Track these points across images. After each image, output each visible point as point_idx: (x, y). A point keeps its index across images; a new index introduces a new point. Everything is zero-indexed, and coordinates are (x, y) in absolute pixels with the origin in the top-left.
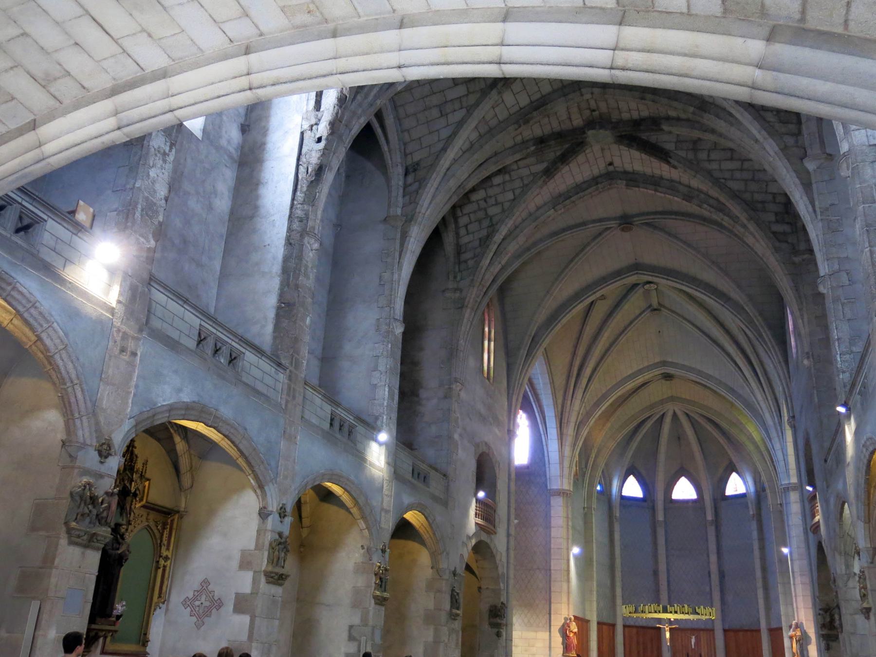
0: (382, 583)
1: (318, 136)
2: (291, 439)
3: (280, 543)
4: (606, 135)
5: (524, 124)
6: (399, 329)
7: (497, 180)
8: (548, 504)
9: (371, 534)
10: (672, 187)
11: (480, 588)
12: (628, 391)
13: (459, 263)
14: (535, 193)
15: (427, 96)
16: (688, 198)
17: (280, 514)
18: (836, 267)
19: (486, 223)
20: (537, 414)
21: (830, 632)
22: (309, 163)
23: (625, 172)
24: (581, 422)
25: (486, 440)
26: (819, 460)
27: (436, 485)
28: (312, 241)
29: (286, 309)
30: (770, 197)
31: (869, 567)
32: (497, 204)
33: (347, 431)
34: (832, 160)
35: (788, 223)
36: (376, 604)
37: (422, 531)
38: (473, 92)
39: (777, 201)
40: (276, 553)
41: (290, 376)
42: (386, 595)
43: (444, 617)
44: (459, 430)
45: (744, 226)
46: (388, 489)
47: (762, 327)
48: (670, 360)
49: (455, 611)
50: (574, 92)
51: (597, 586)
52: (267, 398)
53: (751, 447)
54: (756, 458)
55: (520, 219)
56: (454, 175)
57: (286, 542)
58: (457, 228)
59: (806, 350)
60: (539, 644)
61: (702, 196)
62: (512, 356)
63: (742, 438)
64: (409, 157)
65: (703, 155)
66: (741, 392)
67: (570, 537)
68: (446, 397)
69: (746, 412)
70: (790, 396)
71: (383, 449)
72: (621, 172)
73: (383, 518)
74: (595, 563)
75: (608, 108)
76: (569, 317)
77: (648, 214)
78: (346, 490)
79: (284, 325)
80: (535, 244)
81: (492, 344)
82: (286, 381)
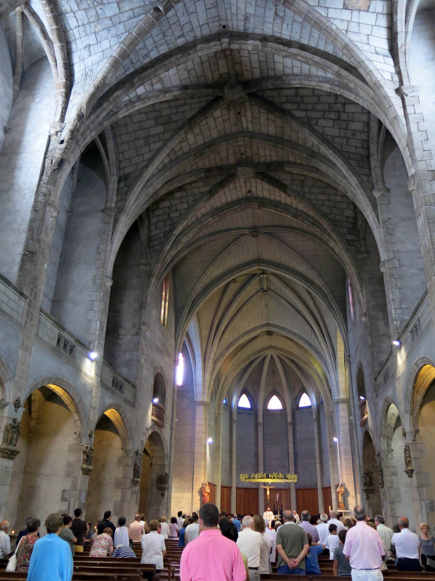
0: (88, 459)
1: (61, 139)
2: (27, 349)
3: (14, 427)
4: (249, 171)
5: (200, 156)
6: (109, 283)
7: (178, 195)
8: (195, 410)
9: (82, 423)
10: (287, 208)
11: (151, 464)
12: (245, 342)
13: (150, 247)
14: (202, 205)
15: (137, 131)
16: (295, 216)
17: (15, 405)
18: (392, 256)
19: (169, 222)
20: (190, 353)
21: (369, 488)
22: (53, 157)
23: (258, 198)
24: (216, 359)
25: (160, 365)
26: (370, 379)
27: (128, 393)
28: (53, 210)
29: (29, 255)
30: (345, 219)
31: (412, 444)
32: (176, 210)
33: (69, 348)
34: (389, 192)
35: (355, 235)
36: (83, 474)
37: (116, 424)
38: (168, 131)
40: (10, 434)
41: (29, 304)
42: (91, 467)
43: (129, 482)
44: (144, 357)
45: (329, 235)
46: (96, 392)
47: (332, 300)
48: (272, 323)
50: (232, 139)
51: (222, 463)
52: (10, 317)
53: (316, 378)
54: (318, 383)
55: (190, 222)
56: (152, 185)
57: (19, 426)
58: (150, 224)
59: (364, 311)
60: (185, 501)
61: (304, 215)
62: (179, 313)
63: (311, 372)
64: (122, 171)
65: (307, 190)
66: (312, 343)
67: (207, 432)
68: (136, 334)
69: (315, 355)
70: (348, 343)
71: (94, 364)
73: (91, 413)
75: (252, 153)
76: (215, 290)
77: (269, 226)
78: (66, 391)
79: (27, 267)
80: (198, 240)
81: (167, 303)
82: (27, 307)
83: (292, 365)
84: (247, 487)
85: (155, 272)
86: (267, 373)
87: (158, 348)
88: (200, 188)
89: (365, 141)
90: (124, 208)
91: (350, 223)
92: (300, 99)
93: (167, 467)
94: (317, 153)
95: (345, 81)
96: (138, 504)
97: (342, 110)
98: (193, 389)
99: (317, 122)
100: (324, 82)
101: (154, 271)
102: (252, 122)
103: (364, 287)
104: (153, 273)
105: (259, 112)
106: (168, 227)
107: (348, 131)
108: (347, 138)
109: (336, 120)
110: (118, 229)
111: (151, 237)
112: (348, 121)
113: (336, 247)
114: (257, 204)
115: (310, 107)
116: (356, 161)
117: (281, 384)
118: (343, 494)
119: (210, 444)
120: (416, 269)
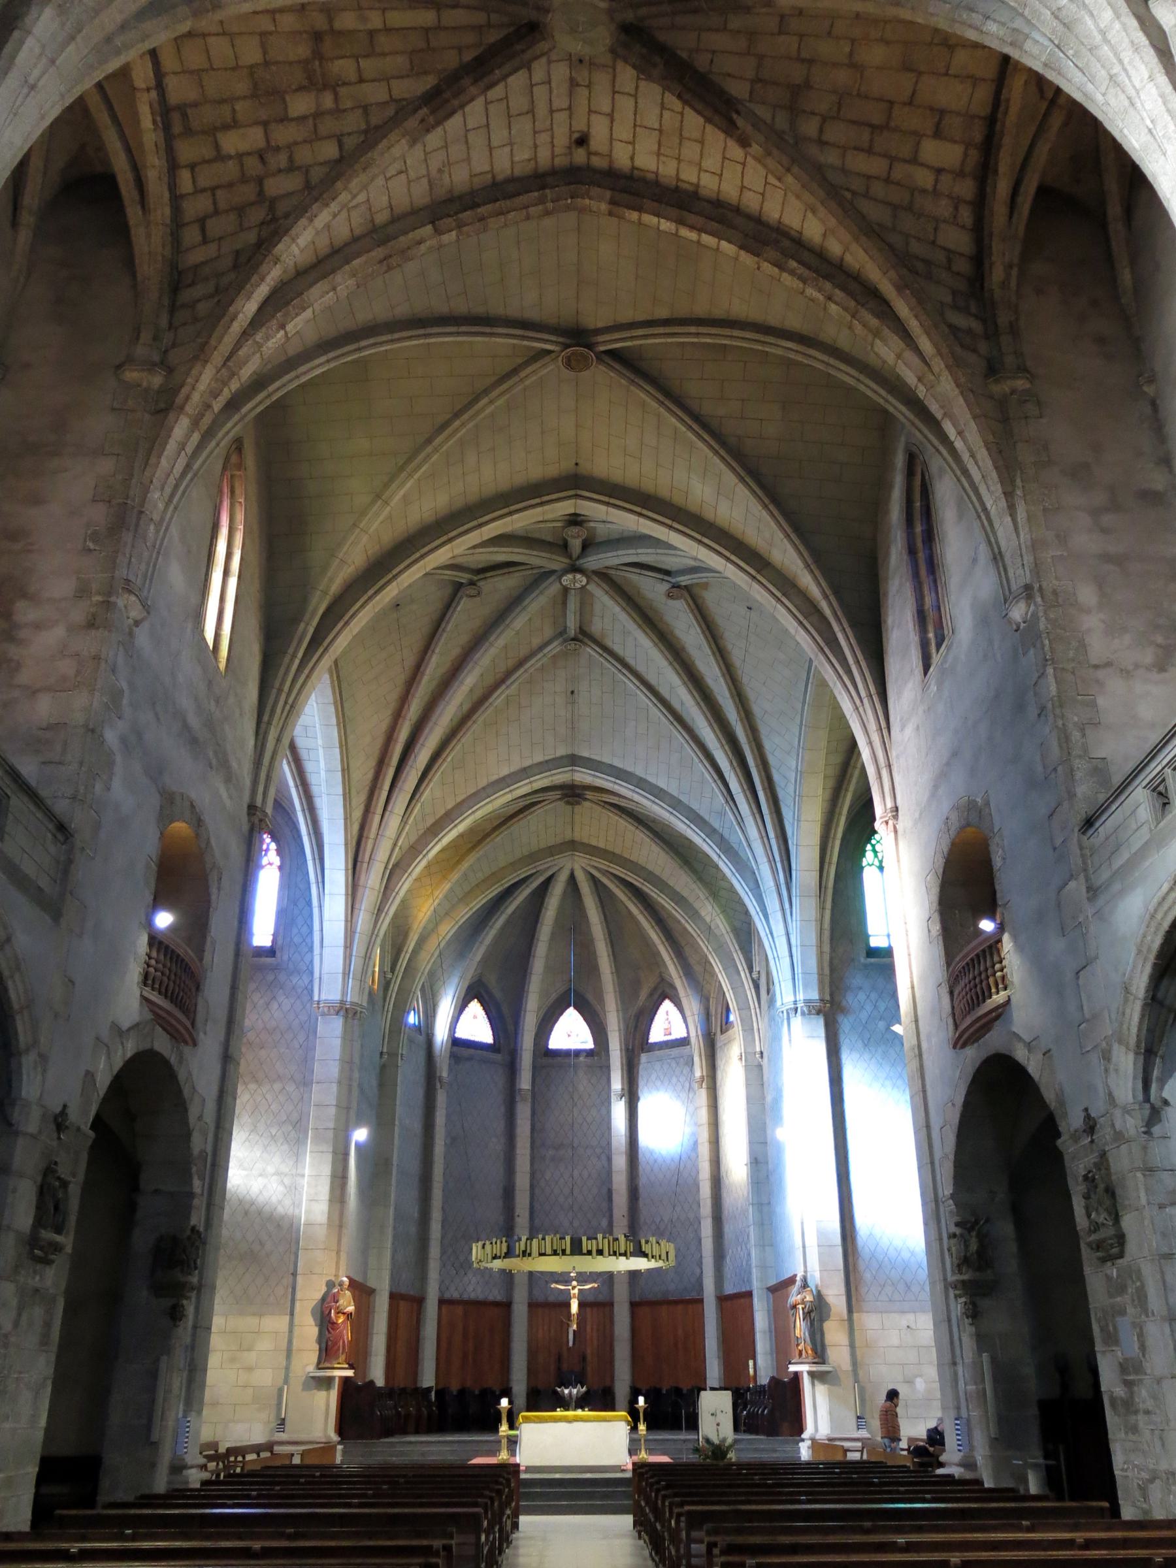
19: (257, 215)
24: (396, 865)
25: (193, 795)
30: (940, 257)
32: (292, 168)
39: (955, 268)
48: (585, 754)
49: (47, 1235)
60: (265, 1344)
61: (786, 243)
65: (810, 127)
66: (716, 825)
67: (354, 1105)
81: (233, 582)
83: (634, 909)
84: (473, 1296)
85: (188, 398)
87: (186, 726)
88: (394, 83)
91: (958, 274)
93: (199, 1203)
96: (54, 1348)
98: (312, 962)
101: (184, 391)
103: (1019, 492)
106: (255, 231)
111: (180, 273)
114: (608, 194)
118: (809, 1312)
119: (357, 1144)
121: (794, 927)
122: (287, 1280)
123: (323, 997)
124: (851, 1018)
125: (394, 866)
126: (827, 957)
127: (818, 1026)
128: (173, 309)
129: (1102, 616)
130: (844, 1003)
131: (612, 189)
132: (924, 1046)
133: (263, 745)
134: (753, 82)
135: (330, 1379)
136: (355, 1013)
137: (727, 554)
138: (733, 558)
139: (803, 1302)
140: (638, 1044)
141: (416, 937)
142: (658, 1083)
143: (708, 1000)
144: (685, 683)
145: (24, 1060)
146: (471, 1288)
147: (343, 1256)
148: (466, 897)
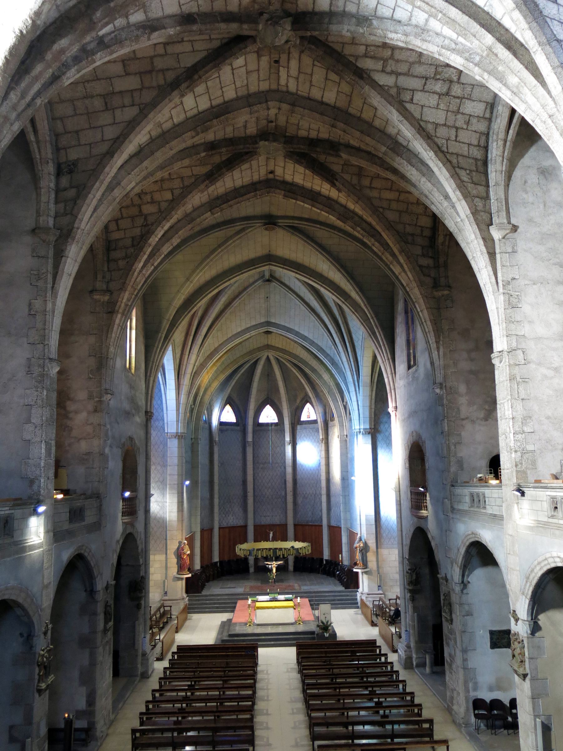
10: (329, 204)
15: (88, 81)
18: (514, 345)
19: (140, 221)
23: (284, 182)
30: (418, 231)
32: (153, 202)
45: (393, 255)
48: (273, 321)
50: (260, 103)
61: (356, 219)
64: (63, 152)
65: (366, 182)
66: (328, 352)
68: (95, 411)
72: (280, 181)
74: (200, 485)
75: (287, 122)
85: (120, 306)
86: (260, 379)
88: (193, 168)
89: (484, 134)
90: (72, 230)
91: (425, 236)
92: (390, 53)
94: (404, 147)
95: (500, 68)
97: (455, 79)
98: (163, 415)
99: (413, 95)
100: (453, 50)
101: (119, 304)
102: (297, 78)
103: (441, 342)
104: (117, 308)
105: (314, 65)
106: (139, 229)
107: (459, 116)
108: (457, 129)
109: (444, 95)
110: (63, 269)
112: (461, 98)
113: (403, 274)
114: (283, 192)
115: (403, 68)
116: (468, 172)
117: (277, 390)
118: (362, 550)
119: (187, 486)
120: (548, 368)
121: (360, 398)
122: (164, 542)
123: (169, 431)
124: (382, 435)
125: (195, 373)
126: (373, 410)
127: (369, 439)
128: (108, 261)
129: (467, 398)
130: (379, 429)
131: (284, 191)
132: (402, 502)
133: (148, 386)
134: (343, 165)
135: (182, 579)
136: (182, 437)
137: (333, 292)
138: (335, 293)
139: (359, 547)
140: (296, 421)
141: (203, 390)
142: (305, 438)
143: (325, 406)
144: (316, 299)
145: (97, 580)
146: (231, 521)
147: (184, 531)
148: (222, 372)
